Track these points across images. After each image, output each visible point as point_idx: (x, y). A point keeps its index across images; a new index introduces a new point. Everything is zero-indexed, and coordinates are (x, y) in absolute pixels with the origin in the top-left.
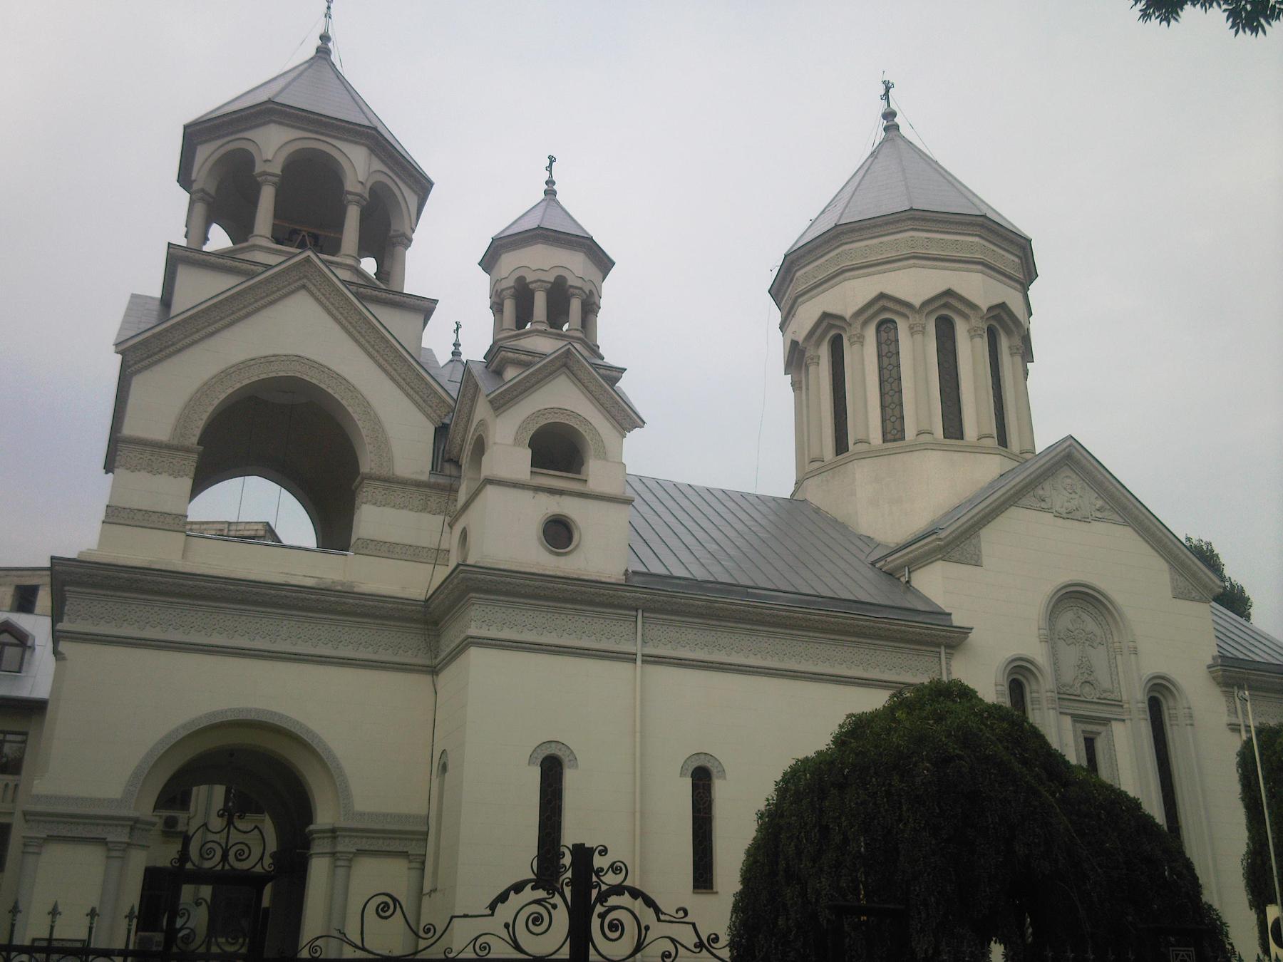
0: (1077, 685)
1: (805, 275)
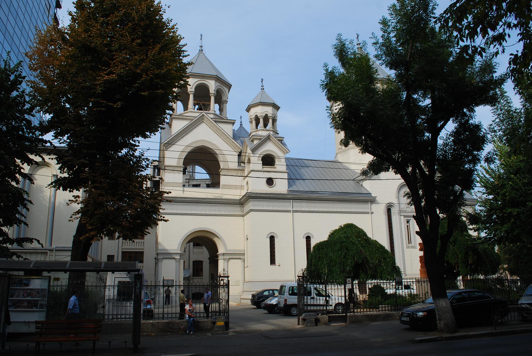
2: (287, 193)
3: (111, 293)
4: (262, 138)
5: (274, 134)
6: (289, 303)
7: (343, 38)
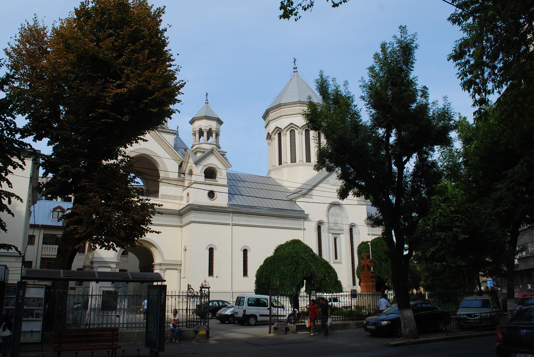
0: (333, 226)
1: (272, 115)
2: (227, 207)
3: (94, 302)
4: (205, 151)
5: (217, 148)
6: (247, 313)
7: (325, 75)
